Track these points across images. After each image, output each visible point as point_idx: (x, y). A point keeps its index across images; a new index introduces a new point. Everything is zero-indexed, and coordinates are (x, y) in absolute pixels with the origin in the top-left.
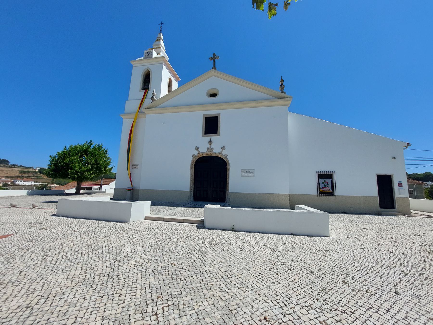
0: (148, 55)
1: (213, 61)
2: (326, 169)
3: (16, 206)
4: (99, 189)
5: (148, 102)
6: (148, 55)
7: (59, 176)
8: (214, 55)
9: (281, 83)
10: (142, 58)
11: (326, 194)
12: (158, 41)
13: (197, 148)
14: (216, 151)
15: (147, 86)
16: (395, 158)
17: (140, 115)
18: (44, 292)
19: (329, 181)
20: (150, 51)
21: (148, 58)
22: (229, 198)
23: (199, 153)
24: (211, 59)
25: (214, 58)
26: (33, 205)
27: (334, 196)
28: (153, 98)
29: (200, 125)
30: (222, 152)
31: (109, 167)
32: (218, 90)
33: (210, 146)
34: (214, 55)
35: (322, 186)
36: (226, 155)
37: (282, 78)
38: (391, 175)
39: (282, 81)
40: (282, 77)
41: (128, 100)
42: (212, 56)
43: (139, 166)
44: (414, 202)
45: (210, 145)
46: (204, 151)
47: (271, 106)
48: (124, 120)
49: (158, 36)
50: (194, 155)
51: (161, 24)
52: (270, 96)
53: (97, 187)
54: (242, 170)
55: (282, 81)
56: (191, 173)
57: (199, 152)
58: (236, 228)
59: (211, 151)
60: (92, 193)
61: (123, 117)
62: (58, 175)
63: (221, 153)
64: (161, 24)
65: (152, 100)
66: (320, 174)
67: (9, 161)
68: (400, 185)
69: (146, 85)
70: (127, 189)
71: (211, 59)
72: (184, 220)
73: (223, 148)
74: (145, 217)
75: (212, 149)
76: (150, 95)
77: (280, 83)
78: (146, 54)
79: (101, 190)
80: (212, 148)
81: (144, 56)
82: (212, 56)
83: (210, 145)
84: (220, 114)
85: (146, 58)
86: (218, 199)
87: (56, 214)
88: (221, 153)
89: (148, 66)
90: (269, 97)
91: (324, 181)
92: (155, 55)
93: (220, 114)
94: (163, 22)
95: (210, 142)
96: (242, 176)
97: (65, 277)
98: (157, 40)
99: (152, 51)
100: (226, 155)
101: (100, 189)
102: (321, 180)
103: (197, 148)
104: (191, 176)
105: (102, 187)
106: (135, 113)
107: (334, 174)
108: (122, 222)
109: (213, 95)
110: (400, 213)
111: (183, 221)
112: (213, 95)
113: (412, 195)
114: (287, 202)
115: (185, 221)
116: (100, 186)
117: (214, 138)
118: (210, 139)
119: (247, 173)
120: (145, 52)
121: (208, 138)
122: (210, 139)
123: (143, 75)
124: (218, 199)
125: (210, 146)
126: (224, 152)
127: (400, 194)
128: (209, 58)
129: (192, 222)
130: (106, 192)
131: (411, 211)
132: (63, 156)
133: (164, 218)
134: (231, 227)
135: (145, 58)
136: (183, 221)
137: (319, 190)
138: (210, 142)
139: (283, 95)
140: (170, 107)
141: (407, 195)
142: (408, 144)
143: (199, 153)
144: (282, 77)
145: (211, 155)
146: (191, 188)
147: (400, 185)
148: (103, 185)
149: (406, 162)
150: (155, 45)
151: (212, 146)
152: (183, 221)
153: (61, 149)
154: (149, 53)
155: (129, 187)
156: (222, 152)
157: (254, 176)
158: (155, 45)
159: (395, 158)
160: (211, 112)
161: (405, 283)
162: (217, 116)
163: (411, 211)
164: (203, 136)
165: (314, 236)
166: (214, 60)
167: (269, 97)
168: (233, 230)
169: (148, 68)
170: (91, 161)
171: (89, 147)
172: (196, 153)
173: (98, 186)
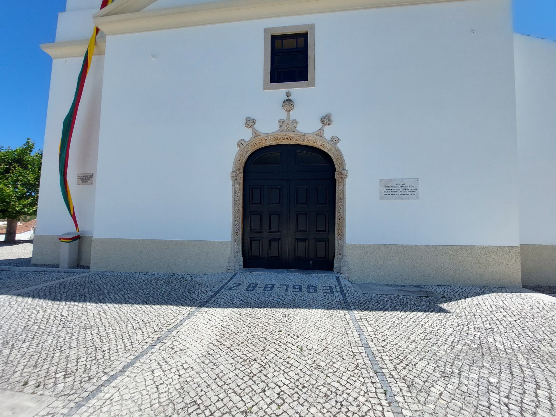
13: (250, 123)
23: (256, 135)
33: (288, 115)
36: (335, 140)
45: (288, 111)
83: (288, 111)
95: (288, 102)
100: (335, 140)
118: (288, 94)
122: (288, 94)
125: (288, 115)
126: (329, 132)
143: (256, 135)
151: (293, 115)
172: (247, 135)
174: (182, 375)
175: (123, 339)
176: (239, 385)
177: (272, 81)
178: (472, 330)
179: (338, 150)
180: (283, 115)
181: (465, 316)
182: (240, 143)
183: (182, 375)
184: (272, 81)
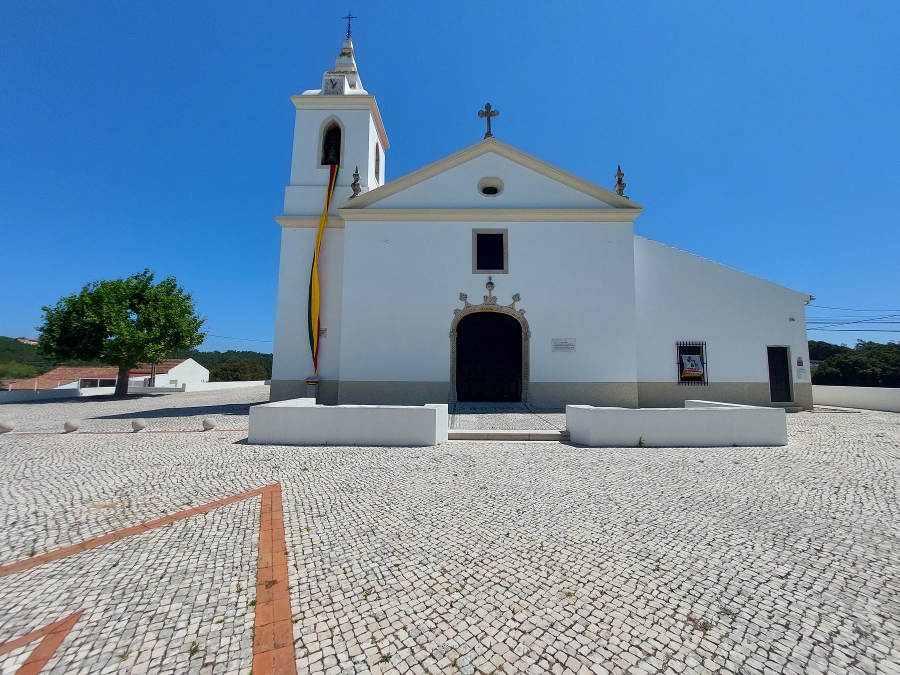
0: (334, 86)
1: (485, 119)
2: (690, 337)
3: (12, 429)
4: (147, 382)
5: (343, 192)
6: (334, 86)
7: (76, 355)
8: (488, 106)
9: (619, 178)
10: (317, 91)
11: (691, 381)
12: (346, 57)
13: (463, 297)
14: (503, 302)
15: (333, 156)
16: (794, 320)
17: (332, 222)
18: (129, 618)
19: (696, 358)
20: (338, 80)
22: (530, 394)
23: (468, 306)
24: (481, 114)
25: (488, 113)
26: (66, 426)
27: (704, 383)
28: (356, 187)
29: (468, 252)
30: (513, 304)
31: (200, 330)
33: (490, 293)
34: (488, 106)
35: (688, 365)
36: (522, 312)
38: (786, 348)
39: (620, 174)
40: (619, 167)
41: (289, 185)
42: (484, 110)
43: (327, 331)
44: (821, 392)
45: (490, 290)
46: (477, 301)
47: (607, 220)
48: (283, 228)
49: (345, 45)
50: (458, 309)
51: (350, 17)
52: (602, 201)
53: (142, 379)
54: (553, 340)
55: (620, 174)
56: (452, 347)
57: (466, 303)
58: (646, 441)
59: (493, 302)
60: (153, 393)
61: (280, 222)
62: (74, 353)
63: (512, 307)
64: (350, 17)
65: (354, 190)
66: (682, 345)
67: (842, 347)
68: (800, 363)
69: (331, 154)
70: (307, 382)
71: (481, 114)
72: (529, 435)
73: (516, 298)
74: (449, 435)
75: (495, 298)
76: (345, 174)
77: (617, 178)
78: (327, 83)
79: (153, 386)
80: (495, 297)
81: (323, 87)
82: (484, 110)
83: (490, 290)
85: (327, 93)
86: (506, 396)
87: (247, 437)
88: (512, 307)
89: (334, 112)
90: (598, 202)
91: (689, 358)
92: (347, 90)
94: (353, 14)
95: (490, 284)
96: (553, 351)
98: (343, 54)
99: (342, 79)
100: (522, 312)
101: (151, 382)
102: (685, 357)
103: (463, 297)
104: (452, 352)
105: (154, 378)
106: (320, 216)
107: (704, 346)
108: (423, 446)
109: (490, 191)
110: (801, 408)
111: (529, 438)
112: (490, 191)
113: (819, 379)
114: (634, 397)
115: (531, 438)
116: (149, 377)
117: (497, 277)
118: (490, 278)
119: (562, 346)
120: (326, 77)
121: (483, 277)
122: (490, 278)
123: (323, 130)
124: (506, 396)
125: (490, 293)
126: (518, 306)
127: (799, 378)
128: (479, 113)
129: (545, 438)
130: (186, 391)
131: (814, 406)
132: (76, 308)
133: (488, 434)
134: (637, 442)
135: (325, 94)
136: (529, 438)
137: (681, 375)
138: (490, 284)
139: (620, 199)
141: (809, 380)
142: (811, 296)
144: (619, 167)
145: (491, 311)
146: (452, 377)
147: (800, 363)
148: (157, 373)
149: (809, 326)
150: (341, 65)
151: (494, 293)
152: (527, 438)
153: (74, 290)
154: (336, 84)
155: (308, 378)
156: (513, 304)
157: (575, 351)
158: (341, 65)
159: (794, 320)
160: (490, 226)
163: (814, 406)
164: (507, 272)
165: (771, 446)
166: (488, 117)
168: (640, 445)
169: (333, 115)
170: (158, 320)
171: (145, 288)
172: (461, 306)
173: (146, 377)
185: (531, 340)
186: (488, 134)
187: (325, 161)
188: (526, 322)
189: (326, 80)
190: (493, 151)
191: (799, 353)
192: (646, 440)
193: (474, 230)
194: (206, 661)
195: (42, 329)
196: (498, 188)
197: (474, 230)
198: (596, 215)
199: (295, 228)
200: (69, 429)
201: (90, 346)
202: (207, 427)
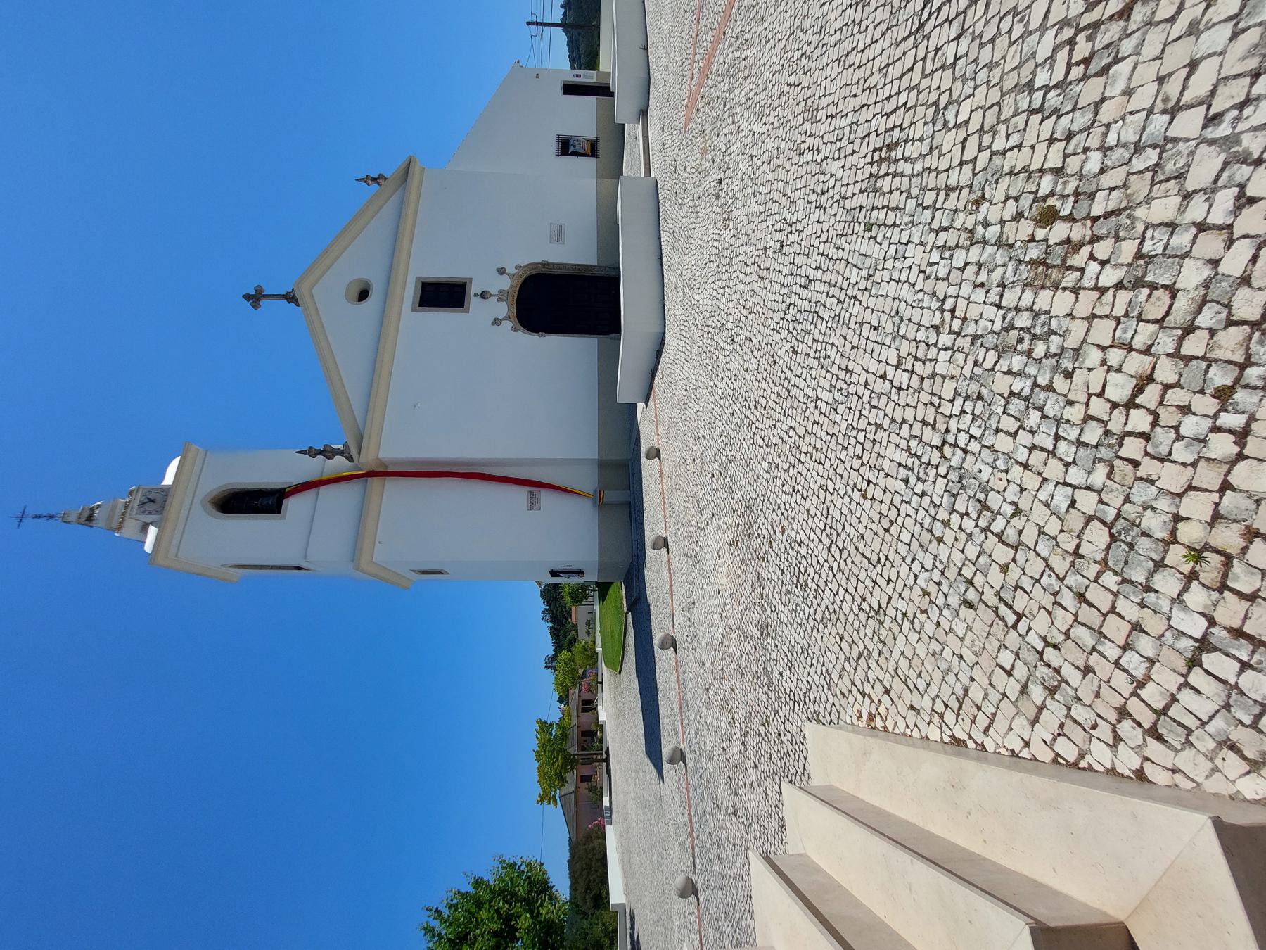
0: (153, 501)
2: (552, 146)
8: (247, 297)
13: (497, 322)
21: (165, 501)
23: (508, 318)
32: (351, 283)
33: (494, 295)
36: (518, 267)
37: (361, 180)
45: (491, 295)
46: (503, 309)
52: (391, 196)
55: (366, 180)
83: (491, 295)
84: (418, 278)
85: (161, 510)
89: (197, 500)
93: (418, 278)
95: (484, 295)
97: (855, 685)
100: (518, 267)
103: (497, 322)
117: (475, 288)
118: (476, 295)
119: (558, 234)
121: (473, 302)
122: (476, 295)
125: (494, 295)
126: (513, 271)
140: (368, 405)
143: (508, 318)
151: (494, 291)
160: (410, 293)
161: (875, 678)
162: (421, 284)
167: (400, 191)
168: (646, 49)
172: (508, 325)
174: (1028, 460)
175: (769, 661)
176: (1242, 360)
177: (421, 305)
178: (881, 203)
179: (526, 266)
180: (493, 300)
181: (880, 206)
182: (514, 329)
183: (1028, 460)
184: (421, 305)
185: (551, 260)
186: (291, 298)
187: (275, 508)
188: (530, 264)
189: (137, 514)
190: (313, 286)
191: (571, 76)
192: (640, 44)
193: (413, 310)
194: (983, 41)
195: (478, 883)
196: (362, 287)
197: (413, 310)
198: (413, 195)
199: (377, 542)
200: (690, 891)
201: (551, 938)
202: (670, 643)
